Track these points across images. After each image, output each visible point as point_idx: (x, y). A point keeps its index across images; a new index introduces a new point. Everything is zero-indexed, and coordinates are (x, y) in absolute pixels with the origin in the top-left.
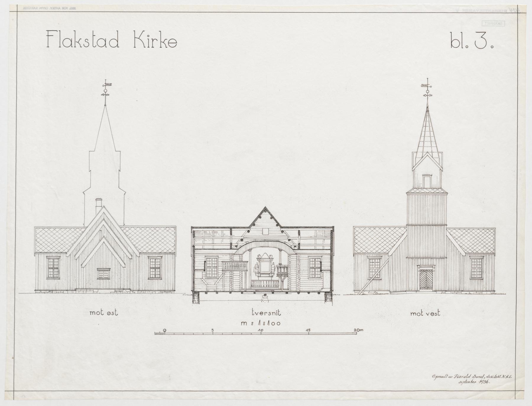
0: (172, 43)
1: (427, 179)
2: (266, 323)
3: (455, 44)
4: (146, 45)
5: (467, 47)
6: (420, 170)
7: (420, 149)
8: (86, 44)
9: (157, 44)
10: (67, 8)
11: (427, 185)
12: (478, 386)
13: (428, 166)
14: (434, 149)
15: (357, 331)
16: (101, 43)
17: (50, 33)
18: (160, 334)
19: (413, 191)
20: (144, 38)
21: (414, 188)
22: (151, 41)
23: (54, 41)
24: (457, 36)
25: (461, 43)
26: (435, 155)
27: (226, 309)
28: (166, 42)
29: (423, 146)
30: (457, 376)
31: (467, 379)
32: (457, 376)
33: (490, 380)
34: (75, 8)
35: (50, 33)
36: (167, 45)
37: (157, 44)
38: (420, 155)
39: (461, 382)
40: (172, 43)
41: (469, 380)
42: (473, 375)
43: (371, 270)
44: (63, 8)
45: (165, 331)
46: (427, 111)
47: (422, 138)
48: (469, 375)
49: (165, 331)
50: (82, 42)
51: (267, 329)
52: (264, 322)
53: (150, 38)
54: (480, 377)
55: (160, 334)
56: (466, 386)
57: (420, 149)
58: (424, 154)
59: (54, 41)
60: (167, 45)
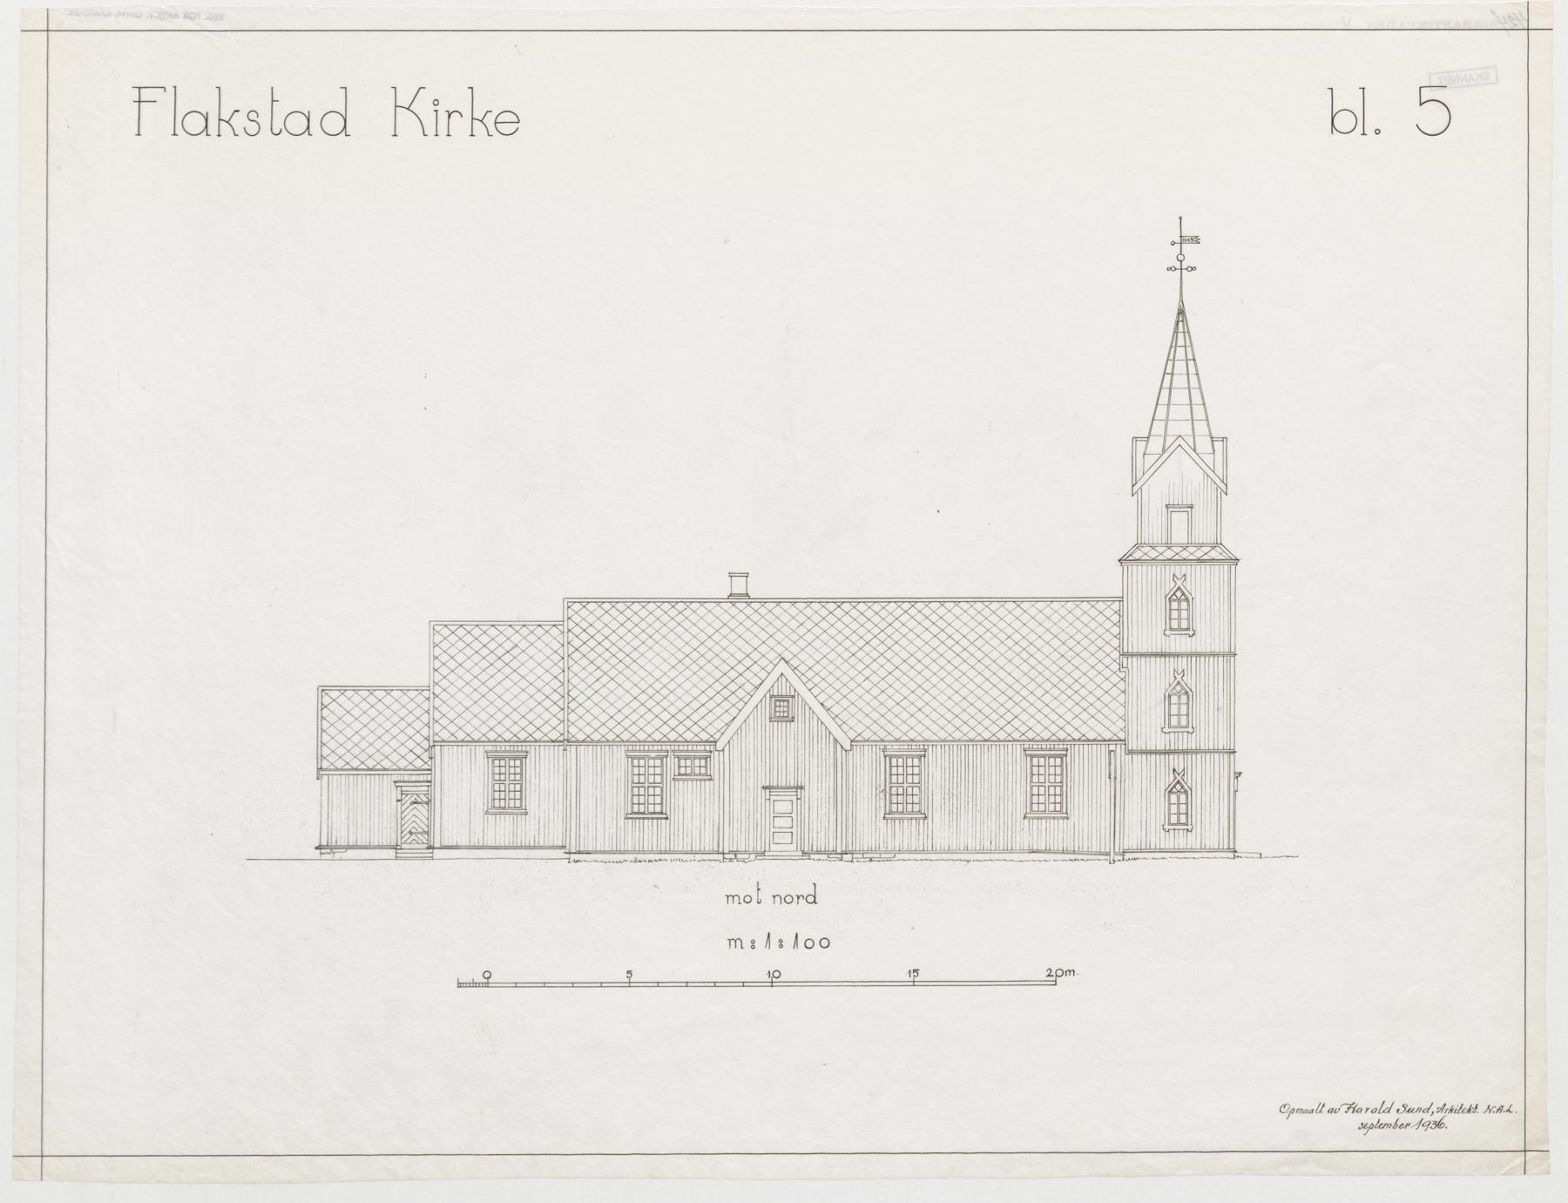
0: (505, 123)
1: (1179, 519)
2: (761, 943)
3: (1344, 122)
4: (430, 130)
5: (1378, 132)
6: (1157, 491)
7: (1158, 428)
8: (253, 128)
9: (460, 125)
10: (220, 17)
11: (1179, 536)
12: (1417, 1138)
13: (1179, 476)
14: (1201, 428)
15: (1053, 977)
16: (297, 123)
17: (146, 95)
18: (474, 985)
19: (1137, 555)
20: (423, 106)
21: (1138, 546)
22: (443, 116)
23: (158, 116)
24: (1348, 98)
25: (1360, 122)
26: (1204, 445)
27: (670, 911)
28: (490, 120)
29: (1167, 420)
30: (1353, 1108)
31: (1382, 1119)
32: (1353, 1108)
33: (1450, 1119)
34: (220, 17)
35: (146, 95)
36: (492, 130)
37: (460, 125)
38: (1155, 445)
39: (1363, 1126)
40: (505, 123)
41: (1388, 1118)
42: (1398, 1105)
43: (1035, 791)
44: (163, 15)
45: (488, 975)
46: (1181, 312)
47: (1165, 393)
48: (1387, 1105)
49: (488, 975)
50: (240, 121)
51: (793, 963)
52: (753, 942)
53: (442, 109)
54: (1419, 1110)
55: (474, 985)
56: (1377, 1138)
57: (1158, 428)
58: (1170, 440)
59: (158, 116)
60: (492, 130)
